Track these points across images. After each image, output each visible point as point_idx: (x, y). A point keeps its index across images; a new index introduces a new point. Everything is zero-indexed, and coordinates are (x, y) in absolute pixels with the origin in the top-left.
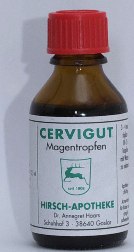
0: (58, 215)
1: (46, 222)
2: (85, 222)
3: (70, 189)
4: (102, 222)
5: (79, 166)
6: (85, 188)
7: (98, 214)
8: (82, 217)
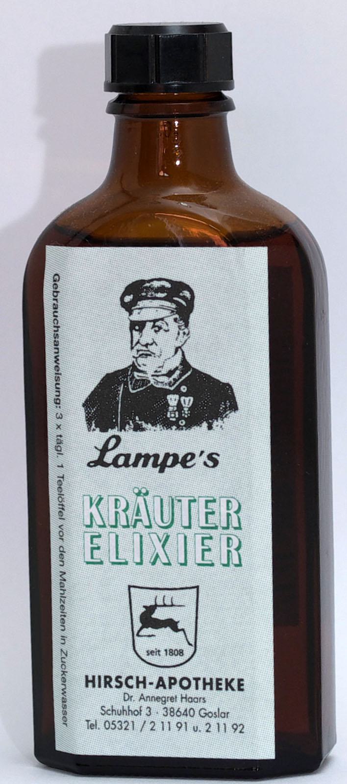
0: (132, 697)
1: (106, 709)
2: (179, 709)
3: (150, 653)
4: (210, 712)
5: (170, 603)
6: (184, 652)
7: (202, 697)
8: (175, 700)
